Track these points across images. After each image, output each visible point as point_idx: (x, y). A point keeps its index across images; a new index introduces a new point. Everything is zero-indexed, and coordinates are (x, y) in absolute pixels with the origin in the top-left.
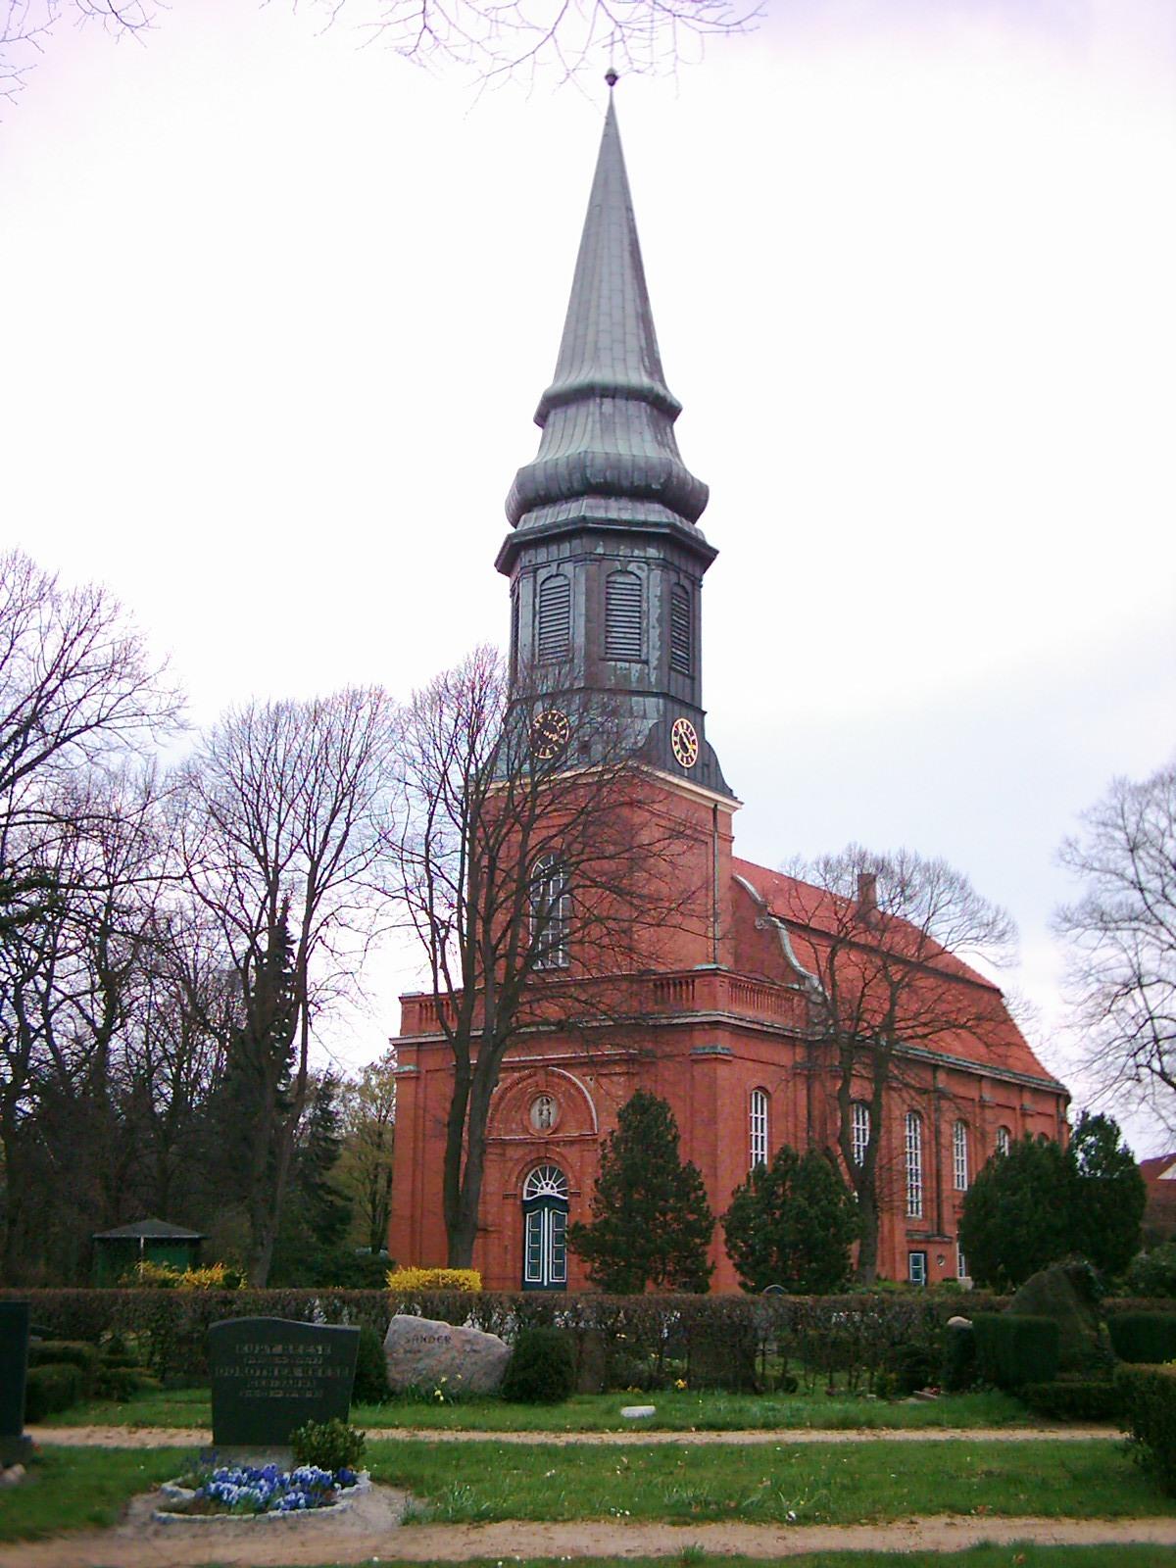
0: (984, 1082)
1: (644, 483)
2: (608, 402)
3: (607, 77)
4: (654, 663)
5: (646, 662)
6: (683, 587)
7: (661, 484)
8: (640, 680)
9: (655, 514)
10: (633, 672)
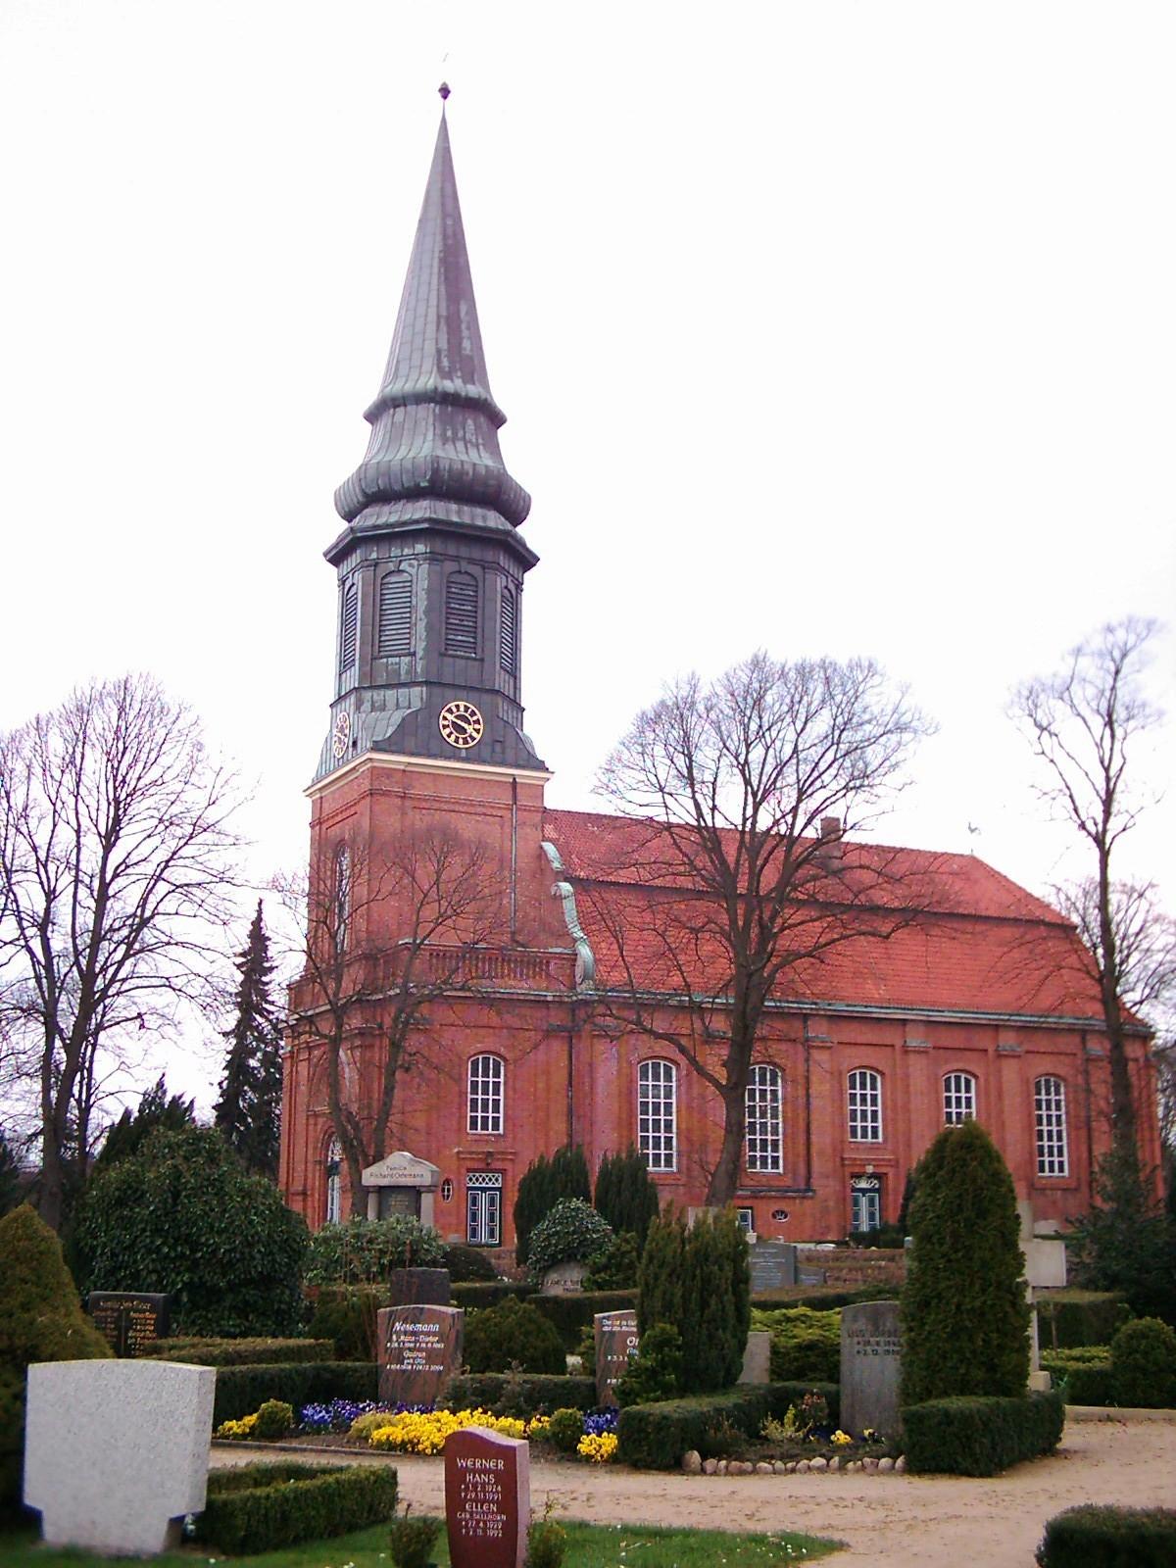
0: (908, 1028)
1: (412, 484)
2: (400, 410)
3: (440, 90)
4: (420, 653)
5: (414, 654)
6: (509, 591)
7: (429, 481)
8: (408, 672)
9: (494, 520)
10: (402, 665)
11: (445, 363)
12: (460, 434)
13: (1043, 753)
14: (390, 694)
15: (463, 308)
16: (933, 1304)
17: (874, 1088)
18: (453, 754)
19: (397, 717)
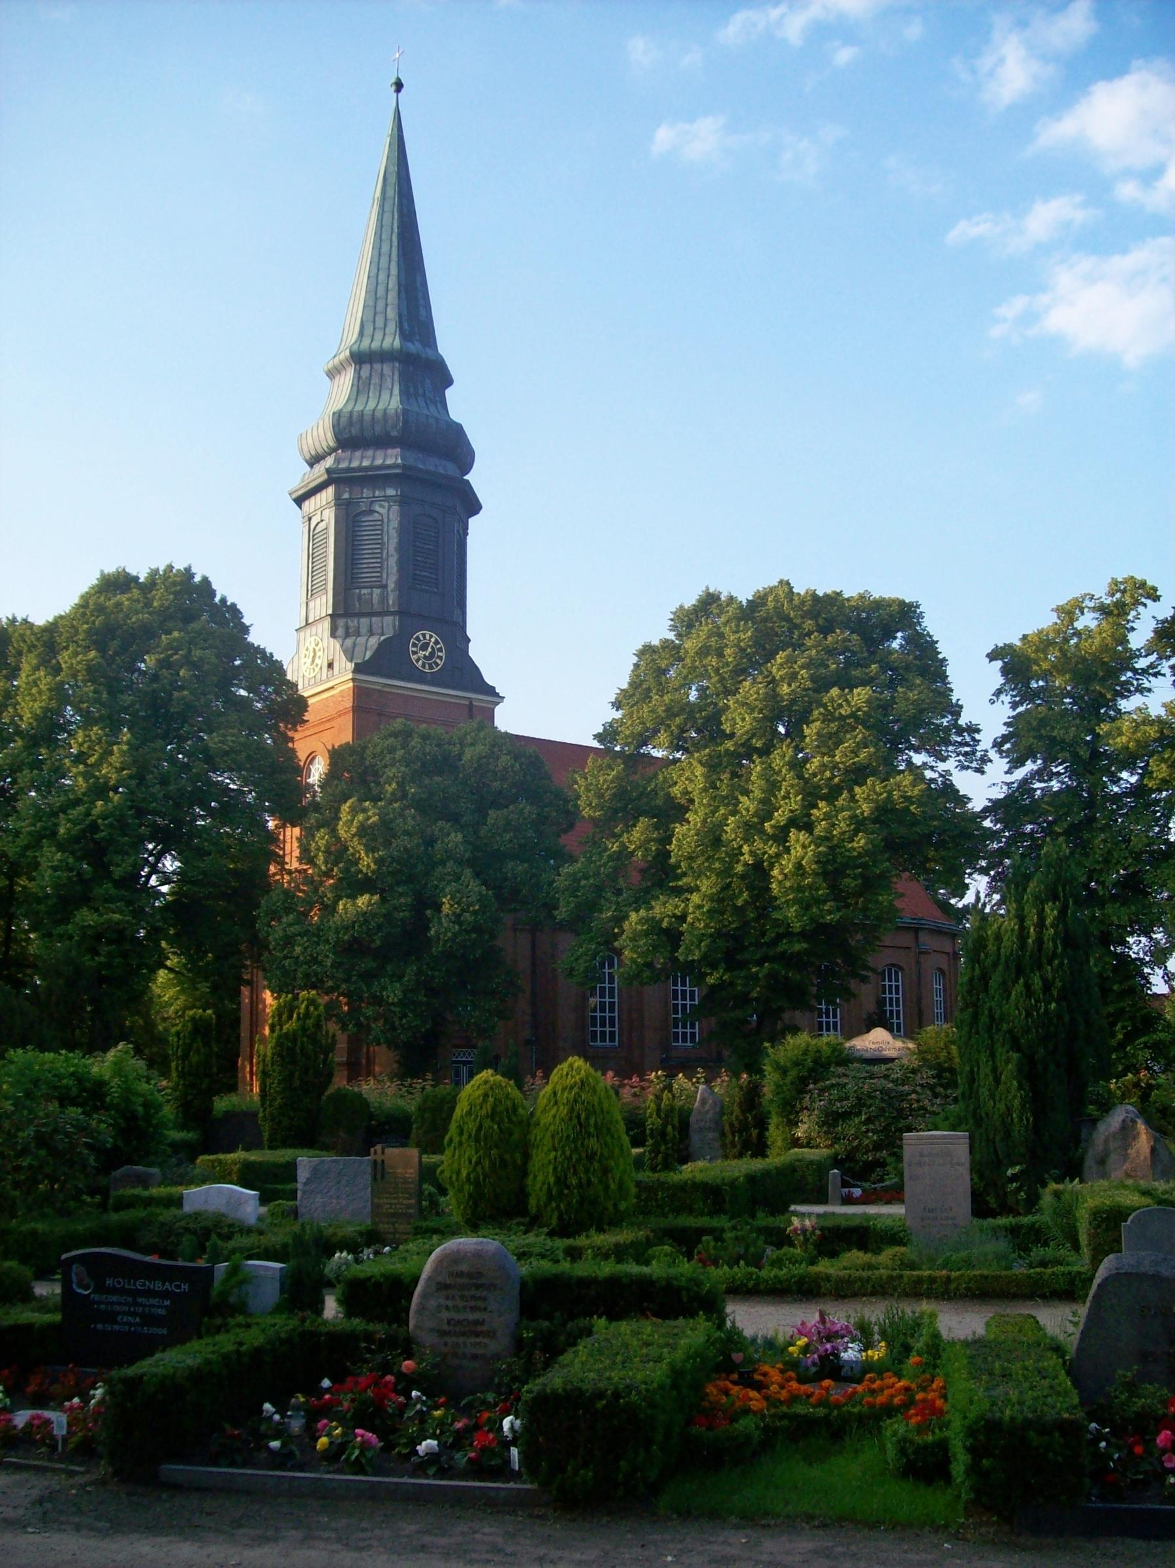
4: (391, 586)
5: (385, 587)
9: (451, 469)
11: (406, 326)
12: (421, 391)
13: (307, 624)
14: (364, 621)
15: (419, 279)
16: (30, 1131)
17: (897, 981)
18: (421, 678)
19: (374, 641)
